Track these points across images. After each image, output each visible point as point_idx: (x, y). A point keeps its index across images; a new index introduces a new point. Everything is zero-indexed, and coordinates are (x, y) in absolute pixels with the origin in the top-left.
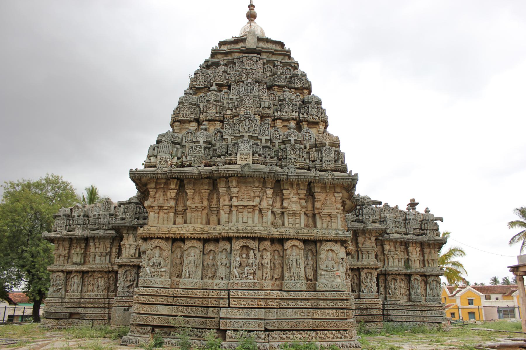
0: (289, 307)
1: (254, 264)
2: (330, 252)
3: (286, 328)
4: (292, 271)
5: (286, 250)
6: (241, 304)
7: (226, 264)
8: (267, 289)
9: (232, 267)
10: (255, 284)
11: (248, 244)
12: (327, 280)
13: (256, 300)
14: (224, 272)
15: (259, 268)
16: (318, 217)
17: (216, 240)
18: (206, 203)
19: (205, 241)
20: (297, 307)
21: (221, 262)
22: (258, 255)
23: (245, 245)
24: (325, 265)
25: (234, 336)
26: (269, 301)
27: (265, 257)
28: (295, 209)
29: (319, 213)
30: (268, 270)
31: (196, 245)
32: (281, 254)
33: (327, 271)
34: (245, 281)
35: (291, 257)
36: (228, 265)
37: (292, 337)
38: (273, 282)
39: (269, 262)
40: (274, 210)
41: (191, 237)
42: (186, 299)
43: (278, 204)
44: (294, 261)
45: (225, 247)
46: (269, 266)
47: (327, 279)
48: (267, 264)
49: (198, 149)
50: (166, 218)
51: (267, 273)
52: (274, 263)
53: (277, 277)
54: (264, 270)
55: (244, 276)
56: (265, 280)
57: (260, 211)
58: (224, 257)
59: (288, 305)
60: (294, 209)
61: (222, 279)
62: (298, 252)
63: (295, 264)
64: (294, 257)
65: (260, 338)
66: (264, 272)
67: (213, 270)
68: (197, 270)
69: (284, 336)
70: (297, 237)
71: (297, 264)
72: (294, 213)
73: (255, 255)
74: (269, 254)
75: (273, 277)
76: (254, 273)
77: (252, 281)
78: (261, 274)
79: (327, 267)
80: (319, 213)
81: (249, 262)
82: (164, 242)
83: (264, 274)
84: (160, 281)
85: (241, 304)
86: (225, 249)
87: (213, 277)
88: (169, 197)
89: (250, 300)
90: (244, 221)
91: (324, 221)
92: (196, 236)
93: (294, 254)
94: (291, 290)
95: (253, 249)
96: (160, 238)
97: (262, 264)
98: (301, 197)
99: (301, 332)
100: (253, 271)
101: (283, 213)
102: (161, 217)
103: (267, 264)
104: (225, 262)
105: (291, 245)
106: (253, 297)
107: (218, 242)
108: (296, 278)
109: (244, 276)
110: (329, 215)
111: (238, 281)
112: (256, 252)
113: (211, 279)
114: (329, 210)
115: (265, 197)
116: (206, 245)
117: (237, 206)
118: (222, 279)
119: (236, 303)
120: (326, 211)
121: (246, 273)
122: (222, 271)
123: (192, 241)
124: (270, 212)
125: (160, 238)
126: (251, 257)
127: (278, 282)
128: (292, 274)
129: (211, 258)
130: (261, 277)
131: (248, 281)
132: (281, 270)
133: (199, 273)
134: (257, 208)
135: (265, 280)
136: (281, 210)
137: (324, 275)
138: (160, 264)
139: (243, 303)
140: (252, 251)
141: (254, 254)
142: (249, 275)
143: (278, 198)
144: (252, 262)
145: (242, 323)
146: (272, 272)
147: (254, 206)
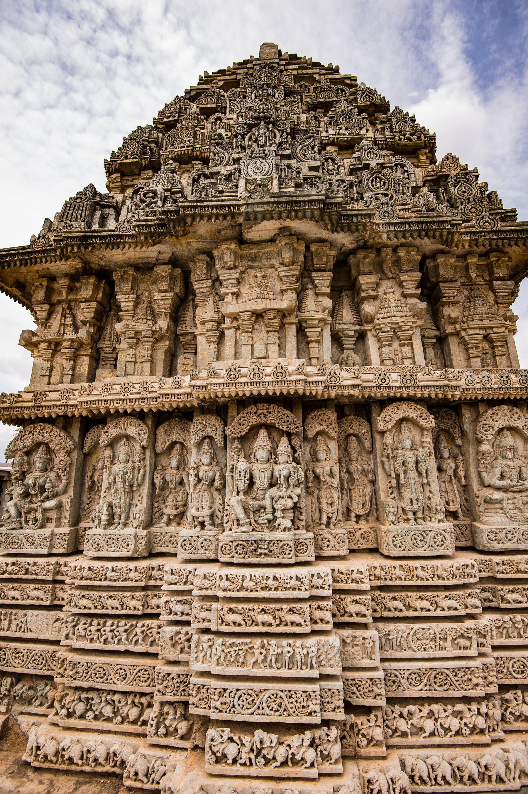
0: (411, 613)
1: (293, 480)
2: (507, 433)
3: (414, 692)
4: (407, 495)
5: (382, 433)
6: (254, 622)
7: (213, 481)
8: (335, 553)
9: (227, 489)
10: (298, 544)
11: (270, 419)
12: (513, 519)
13: (305, 606)
14: (206, 505)
15: (307, 488)
16: (454, 345)
17: (184, 415)
18: (163, 323)
19: (159, 418)
20: (439, 613)
21: (197, 475)
22: (304, 453)
23: (263, 421)
24: (498, 471)
25: (231, 750)
26: (349, 598)
27: (322, 455)
28: (398, 319)
29: (457, 334)
30: (336, 494)
31: (131, 431)
32: (367, 444)
33: (505, 490)
34: (268, 536)
35: (399, 452)
36: (217, 483)
37: (429, 725)
38: (352, 525)
39: (336, 470)
40: (339, 327)
41: (117, 411)
42: (97, 594)
43: (347, 315)
44: (411, 464)
45: (208, 431)
46: (336, 482)
47: (512, 513)
48: (331, 475)
49: (148, 200)
50: (68, 370)
51: (331, 504)
52: (348, 472)
53: (360, 512)
54: (323, 494)
55: (263, 518)
56: (328, 525)
57: (301, 330)
58: (206, 459)
59: (409, 607)
60: (394, 320)
61: (202, 524)
62: (417, 438)
63: (413, 474)
64: (408, 453)
65: (326, 757)
66: (324, 501)
67: (181, 496)
68: (135, 501)
69: (402, 725)
70: (412, 392)
71: (420, 474)
72: (396, 329)
73: (295, 451)
74: (333, 445)
75: (348, 510)
76: (296, 508)
77: (289, 535)
78: (315, 506)
79: (502, 477)
80: (457, 334)
81: (276, 473)
82: (56, 431)
83: (324, 506)
84: (39, 536)
85: (254, 622)
86: (210, 438)
87: (180, 517)
88: (80, 317)
89: (286, 607)
90: (256, 354)
91: (473, 352)
92: (128, 407)
93: (407, 443)
94: (412, 554)
95: (289, 435)
96: (44, 420)
97: (317, 477)
98: (406, 292)
99: (459, 707)
100: (289, 503)
101: (362, 336)
102: (57, 368)
103: (331, 475)
104: (211, 474)
105: (397, 417)
106: (296, 594)
107: (190, 419)
108: (420, 515)
109: (263, 518)
110: (486, 337)
111: (244, 537)
112: (296, 441)
113: (174, 524)
114: (487, 323)
115: (310, 292)
116: (161, 431)
117: (235, 317)
118: (202, 524)
119: (238, 618)
120: (477, 323)
121: (269, 509)
122: (199, 505)
123: (122, 420)
124: (327, 334)
125: (44, 420)
126: (282, 458)
127: (364, 525)
128: (406, 504)
129: (174, 463)
130: (316, 516)
131: (278, 535)
132: (369, 490)
133: (140, 507)
134: (292, 319)
135: (328, 525)
136: (357, 327)
137: (499, 501)
138: (43, 489)
139: (261, 618)
140: (284, 439)
141: (292, 447)
142: (278, 514)
143: (346, 302)
144: (285, 472)
145: (264, 697)
146: (346, 497)
147: (283, 314)
